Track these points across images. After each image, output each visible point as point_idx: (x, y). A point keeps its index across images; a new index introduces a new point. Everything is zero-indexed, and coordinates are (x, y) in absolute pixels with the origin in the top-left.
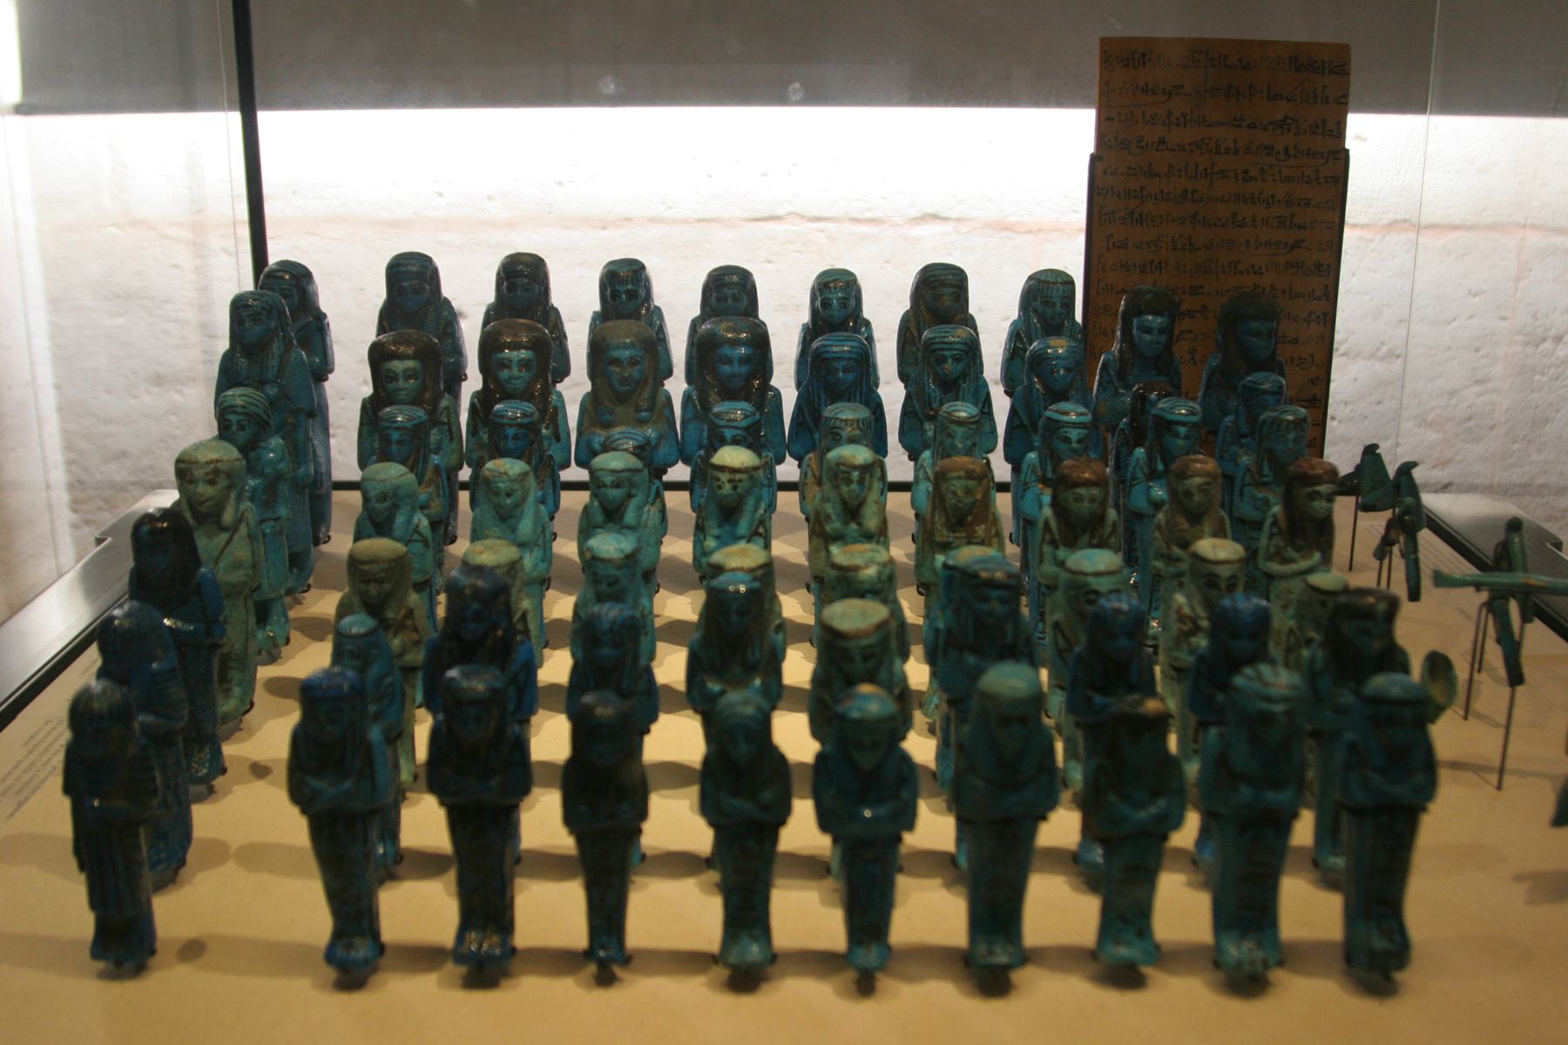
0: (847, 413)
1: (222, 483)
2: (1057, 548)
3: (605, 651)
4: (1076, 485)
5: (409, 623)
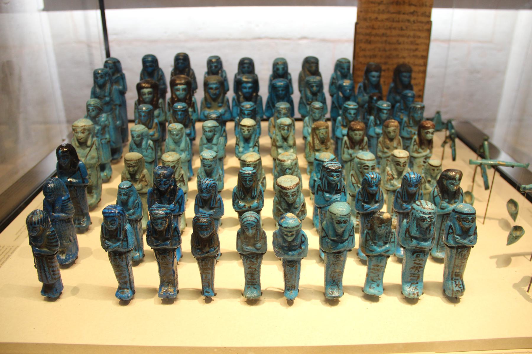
0: (282, 106)
1: (87, 133)
3: (205, 195)
4: (355, 130)
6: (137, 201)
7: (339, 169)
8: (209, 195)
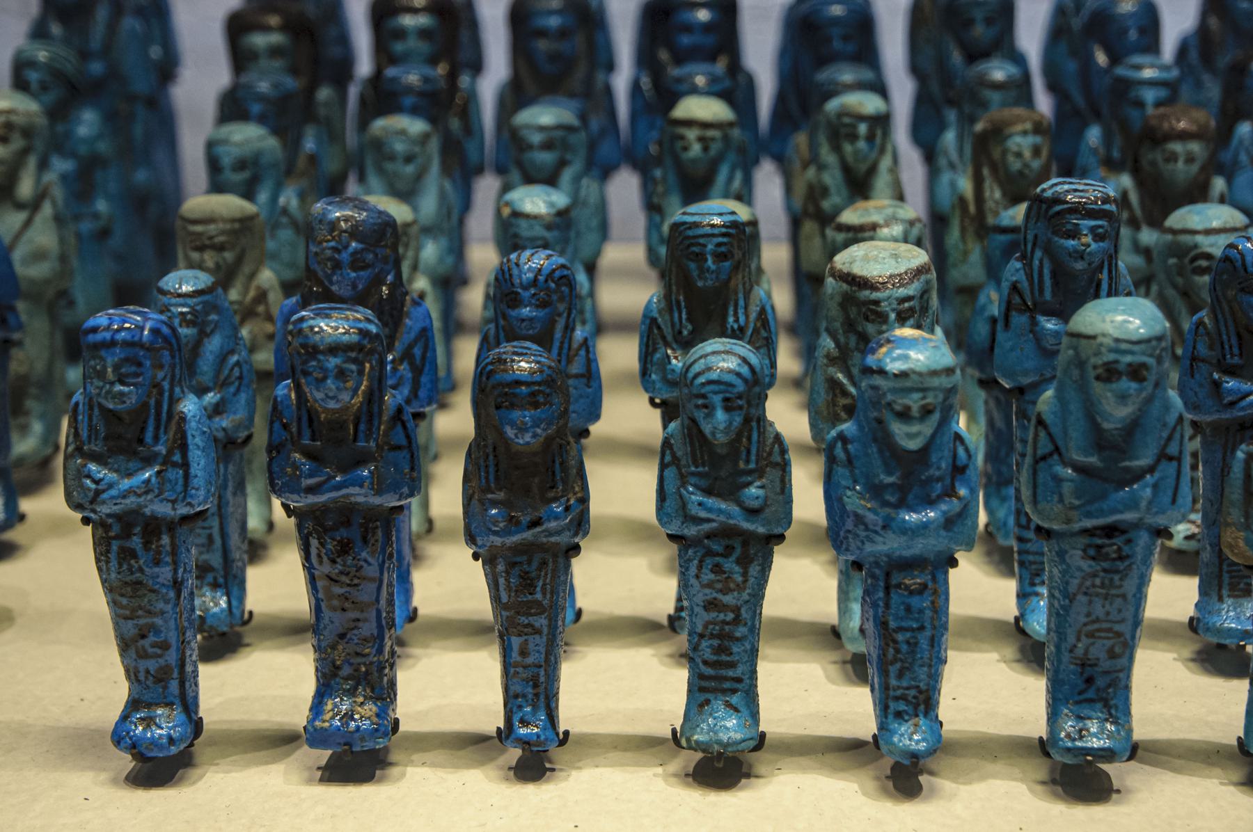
5: (261, 309)
6: (235, 358)
7: (1103, 203)
8: (540, 313)
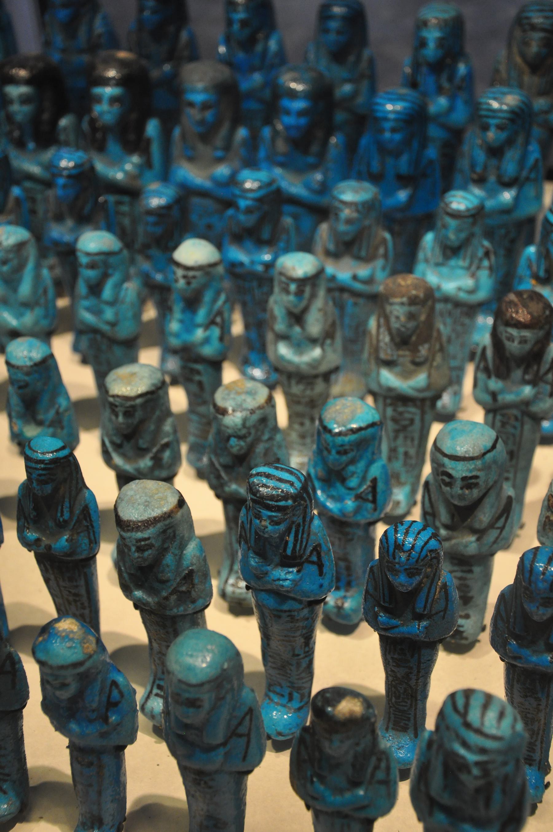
2: (489, 377)
